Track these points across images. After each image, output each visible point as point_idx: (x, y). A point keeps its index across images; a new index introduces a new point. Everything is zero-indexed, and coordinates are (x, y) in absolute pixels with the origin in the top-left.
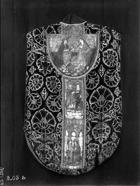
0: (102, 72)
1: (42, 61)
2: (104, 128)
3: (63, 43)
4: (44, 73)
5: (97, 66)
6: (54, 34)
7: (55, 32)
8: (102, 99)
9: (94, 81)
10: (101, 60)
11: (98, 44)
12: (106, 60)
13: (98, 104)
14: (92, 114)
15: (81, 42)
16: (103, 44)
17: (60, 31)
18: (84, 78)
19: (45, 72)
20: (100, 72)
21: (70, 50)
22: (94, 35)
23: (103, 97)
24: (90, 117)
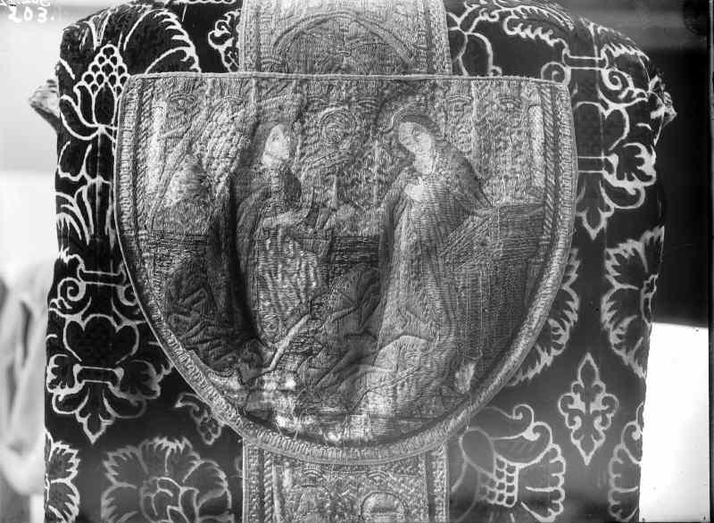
0: (588, 419)
1: (69, 318)
2: (127, 323)
3: (249, 155)
4: (84, 421)
5: (546, 359)
6: (181, 76)
7: (191, 51)
8: (113, 80)
9: (515, 483)
10: (590, 312)
11: (564, 165)
12: (627, 322)
13: (78, 109)
15: (412, 149)
16: (605, 173)
17: (233, 49)
18: (429, 458)
19: (94, 409)
20: (574, 413)
21: (310, 220)
22: (530, 88)
23: (120, 62)
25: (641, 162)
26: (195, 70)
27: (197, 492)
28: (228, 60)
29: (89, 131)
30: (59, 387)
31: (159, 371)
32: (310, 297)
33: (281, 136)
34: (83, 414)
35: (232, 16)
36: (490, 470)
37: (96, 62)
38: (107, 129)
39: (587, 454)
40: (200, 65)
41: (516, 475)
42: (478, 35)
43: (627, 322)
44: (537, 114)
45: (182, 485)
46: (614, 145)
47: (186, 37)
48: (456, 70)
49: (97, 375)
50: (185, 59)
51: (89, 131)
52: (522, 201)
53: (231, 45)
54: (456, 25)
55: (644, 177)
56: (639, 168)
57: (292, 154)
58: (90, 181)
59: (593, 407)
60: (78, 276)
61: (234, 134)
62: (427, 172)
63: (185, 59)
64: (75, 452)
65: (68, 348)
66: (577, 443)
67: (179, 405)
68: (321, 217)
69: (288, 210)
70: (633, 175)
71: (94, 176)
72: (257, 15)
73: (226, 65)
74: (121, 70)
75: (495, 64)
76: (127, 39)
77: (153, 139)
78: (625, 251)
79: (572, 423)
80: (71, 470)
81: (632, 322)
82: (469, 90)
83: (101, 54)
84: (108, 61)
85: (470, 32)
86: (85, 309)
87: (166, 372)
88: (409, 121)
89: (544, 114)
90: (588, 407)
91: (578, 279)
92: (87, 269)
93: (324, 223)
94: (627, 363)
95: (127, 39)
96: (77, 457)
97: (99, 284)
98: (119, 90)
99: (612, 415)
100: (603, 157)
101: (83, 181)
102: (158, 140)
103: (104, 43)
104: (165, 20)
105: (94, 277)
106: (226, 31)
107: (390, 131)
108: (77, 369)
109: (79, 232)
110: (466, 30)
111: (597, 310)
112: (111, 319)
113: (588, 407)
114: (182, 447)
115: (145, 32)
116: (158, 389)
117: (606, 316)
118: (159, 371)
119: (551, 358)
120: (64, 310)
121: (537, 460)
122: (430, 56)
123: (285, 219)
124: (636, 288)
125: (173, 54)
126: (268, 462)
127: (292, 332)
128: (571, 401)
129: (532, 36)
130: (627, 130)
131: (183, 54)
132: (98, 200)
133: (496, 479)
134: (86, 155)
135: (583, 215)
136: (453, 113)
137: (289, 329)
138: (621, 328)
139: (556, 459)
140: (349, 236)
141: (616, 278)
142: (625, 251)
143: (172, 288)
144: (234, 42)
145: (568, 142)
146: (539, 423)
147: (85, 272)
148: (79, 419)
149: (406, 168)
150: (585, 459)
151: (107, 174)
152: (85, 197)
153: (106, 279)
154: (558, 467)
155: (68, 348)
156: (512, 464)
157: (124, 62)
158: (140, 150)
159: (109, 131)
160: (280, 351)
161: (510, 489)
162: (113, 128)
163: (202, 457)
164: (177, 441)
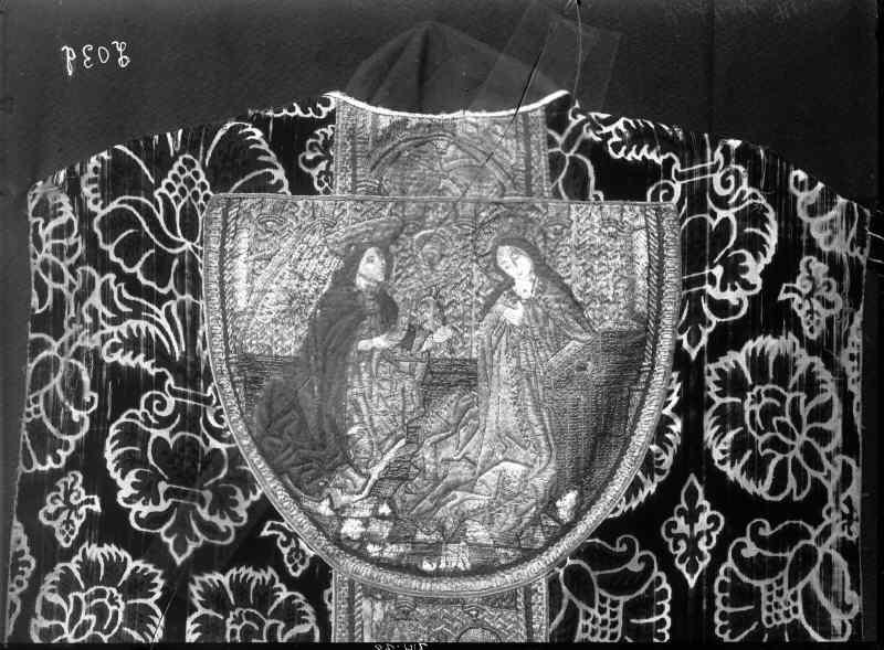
0: (693, 542)
1: (155, 433)
4: (170, 541)
7: (279, 174)
9: (619, 618)
10: (693, 433)
12: (730, 435)
13: (160, 217)
14: (107, 297)
15: (511, 272)
16: (708, 287)
17: (327, 173)
18: (529, 592)
19: (182, 530)
21: (406, 344)
23: (203, 178)
24: (88, 319)
25: (745, 270)
26: (285, 193)
27: (282, 625)
28: (320, 184)
29: (174, 244)
30: (140, 502)
31: (246, 497)
32: (406, 421)
33: (377, 259)
34: (168, 534)
35: (326, 135)
36: (592, 606)
37: (175, 170)
38: (193, 246)
39: (692, 577)
40: (290, 188)
41: (620, 609)
42: (579, 156)
43: (730, 435)
44: (641, 238)
45: (266, 617)
46: (719, 257)
47: (273, 157)
48: (556, 194)
49: (184, 495)
50: (273, 182)
51: (174, 244)
52: (624, 327)
53: (324, 169)
54: (557, 146)
55: (747, 286)
56: (743, 276)
57: (387, 277)
58: (179, 297)
59: (698, 528)
60: (166, 390)
61: (326, 256)
62: (525, 296)
63: (273, 182)
64: (160, 572)
65: (152, 462)
66: (682, 567)
67: (265, 533)
68: (418, 340)
69: (383, 333)
70: (736, 284)
71: (183, 293)
72: (352, 137)
73: (318, 188)
74: (203, 186)
75: (596, 188)
76: (209, 154)
77: (239, 262)
78: (726, 364)
79: (676, 547)
80: (155, 590)
81: (735, 436)
82: (569, 214)
83: (179, 163)
84: (189, 174)
85: (572, 153)
86: (173, 426)
87: (254, 498)
88: (509, 244)
89: (648, 237)
90: (692, 529)
91: (679, 402)
92: (176, 385)
93: (421, 347)
94: (732, 478)
95: (209, 154)
96: (162, 577)
97: (188, 402)
98: (202, 208)
99: (717, 532)
100: (707, 272)
101: (171, 296)
102: (245, 262)
103: (182, 152)
104: (249, 138)
105: (184, 395)
106: (319, 153)
107: (487, 254)
108: (163, 487)
109: (167, 345)
110: (568, 151)
111: (700, 431)
112: (200, 439)
113: (692, 529)
114: (267, 578)
115: (229, 146)
116: (244, 514)
117: (709, 433)
118: (246, 497)
119: (655, 486)
120: (148, 423)
121: (642, 591)
122: (528, 178)
123: (380, 342)
124: (739, 400)
125: (258, 176)
126: (359, 595)
127: (390, 456)
128: (674, 525)
129: (639, 158)
130: (733, 238)
131: (271, 177)
132: (188, 318)
133: (598, 615)
134: (173, 270)
135: (684, 337)
136: (552, 236)
137: (384, 454)
138: (725, 443)
139: (661, 587)
140: (446, 359)
141: (717, 393)
142: (726, 364)
143: (264, 410)
144: (328, 166)
145: (672, 262)
146: (644, 553)
147: (174, 387)
148: (165, 539)
149: (506, 292)
150: (689, 582)
151: (196, 293)
152: (174, 311)
153: (196, 398)
154: (663, 594)
155: (152, 462)
156: (616, 598)
157: (207, 178)
158: (226, 272)
159: (196, 250)
160: (375, 476)
161: (614, 624)
162: (200, 248)
163: (289, 589)
164: (262, 571)
